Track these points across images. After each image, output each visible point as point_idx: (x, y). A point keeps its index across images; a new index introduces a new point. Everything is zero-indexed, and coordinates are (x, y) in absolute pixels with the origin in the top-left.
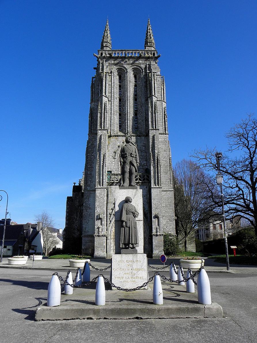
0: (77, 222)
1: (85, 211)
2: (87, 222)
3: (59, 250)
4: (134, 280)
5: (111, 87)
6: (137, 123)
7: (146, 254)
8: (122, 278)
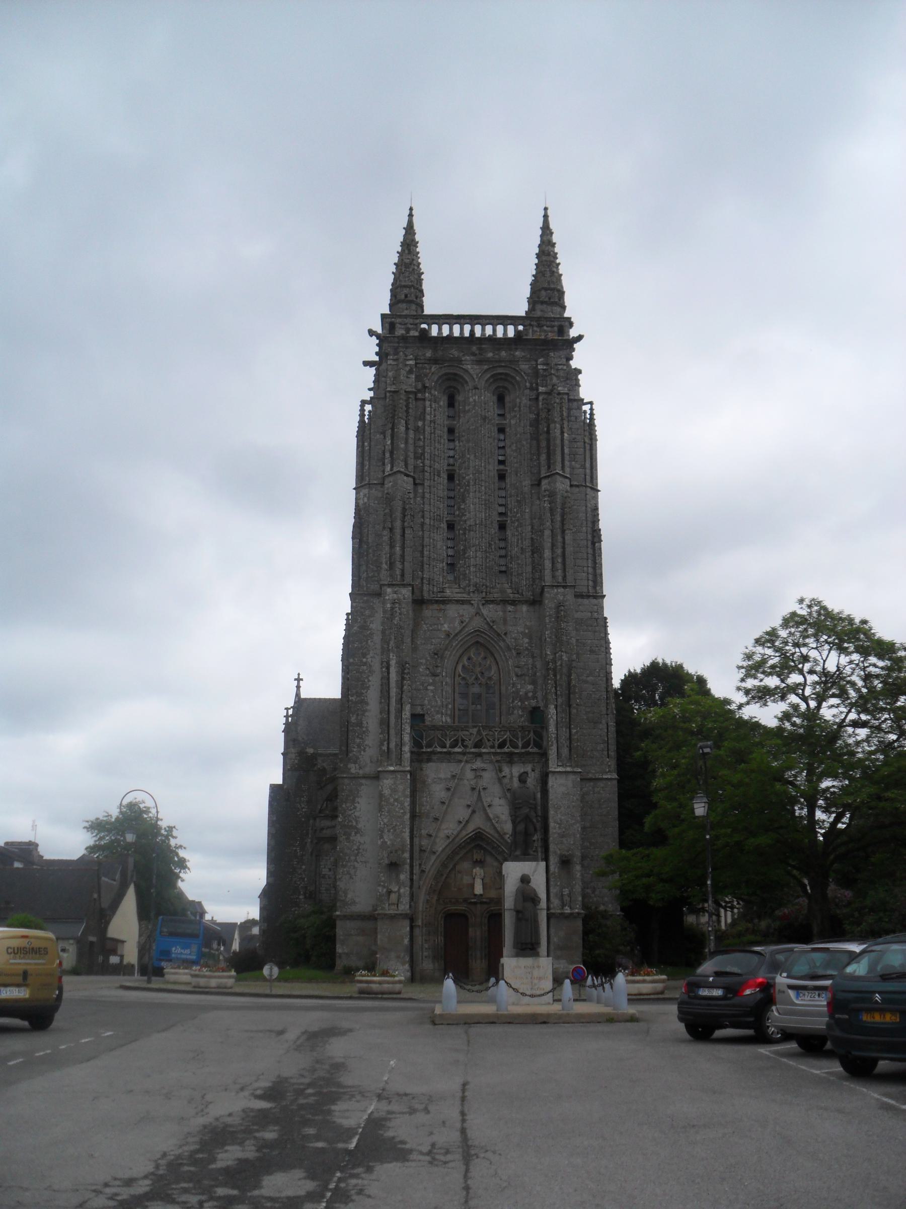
1: (342, 838)
2: (350, 874)
6: (505, 556)
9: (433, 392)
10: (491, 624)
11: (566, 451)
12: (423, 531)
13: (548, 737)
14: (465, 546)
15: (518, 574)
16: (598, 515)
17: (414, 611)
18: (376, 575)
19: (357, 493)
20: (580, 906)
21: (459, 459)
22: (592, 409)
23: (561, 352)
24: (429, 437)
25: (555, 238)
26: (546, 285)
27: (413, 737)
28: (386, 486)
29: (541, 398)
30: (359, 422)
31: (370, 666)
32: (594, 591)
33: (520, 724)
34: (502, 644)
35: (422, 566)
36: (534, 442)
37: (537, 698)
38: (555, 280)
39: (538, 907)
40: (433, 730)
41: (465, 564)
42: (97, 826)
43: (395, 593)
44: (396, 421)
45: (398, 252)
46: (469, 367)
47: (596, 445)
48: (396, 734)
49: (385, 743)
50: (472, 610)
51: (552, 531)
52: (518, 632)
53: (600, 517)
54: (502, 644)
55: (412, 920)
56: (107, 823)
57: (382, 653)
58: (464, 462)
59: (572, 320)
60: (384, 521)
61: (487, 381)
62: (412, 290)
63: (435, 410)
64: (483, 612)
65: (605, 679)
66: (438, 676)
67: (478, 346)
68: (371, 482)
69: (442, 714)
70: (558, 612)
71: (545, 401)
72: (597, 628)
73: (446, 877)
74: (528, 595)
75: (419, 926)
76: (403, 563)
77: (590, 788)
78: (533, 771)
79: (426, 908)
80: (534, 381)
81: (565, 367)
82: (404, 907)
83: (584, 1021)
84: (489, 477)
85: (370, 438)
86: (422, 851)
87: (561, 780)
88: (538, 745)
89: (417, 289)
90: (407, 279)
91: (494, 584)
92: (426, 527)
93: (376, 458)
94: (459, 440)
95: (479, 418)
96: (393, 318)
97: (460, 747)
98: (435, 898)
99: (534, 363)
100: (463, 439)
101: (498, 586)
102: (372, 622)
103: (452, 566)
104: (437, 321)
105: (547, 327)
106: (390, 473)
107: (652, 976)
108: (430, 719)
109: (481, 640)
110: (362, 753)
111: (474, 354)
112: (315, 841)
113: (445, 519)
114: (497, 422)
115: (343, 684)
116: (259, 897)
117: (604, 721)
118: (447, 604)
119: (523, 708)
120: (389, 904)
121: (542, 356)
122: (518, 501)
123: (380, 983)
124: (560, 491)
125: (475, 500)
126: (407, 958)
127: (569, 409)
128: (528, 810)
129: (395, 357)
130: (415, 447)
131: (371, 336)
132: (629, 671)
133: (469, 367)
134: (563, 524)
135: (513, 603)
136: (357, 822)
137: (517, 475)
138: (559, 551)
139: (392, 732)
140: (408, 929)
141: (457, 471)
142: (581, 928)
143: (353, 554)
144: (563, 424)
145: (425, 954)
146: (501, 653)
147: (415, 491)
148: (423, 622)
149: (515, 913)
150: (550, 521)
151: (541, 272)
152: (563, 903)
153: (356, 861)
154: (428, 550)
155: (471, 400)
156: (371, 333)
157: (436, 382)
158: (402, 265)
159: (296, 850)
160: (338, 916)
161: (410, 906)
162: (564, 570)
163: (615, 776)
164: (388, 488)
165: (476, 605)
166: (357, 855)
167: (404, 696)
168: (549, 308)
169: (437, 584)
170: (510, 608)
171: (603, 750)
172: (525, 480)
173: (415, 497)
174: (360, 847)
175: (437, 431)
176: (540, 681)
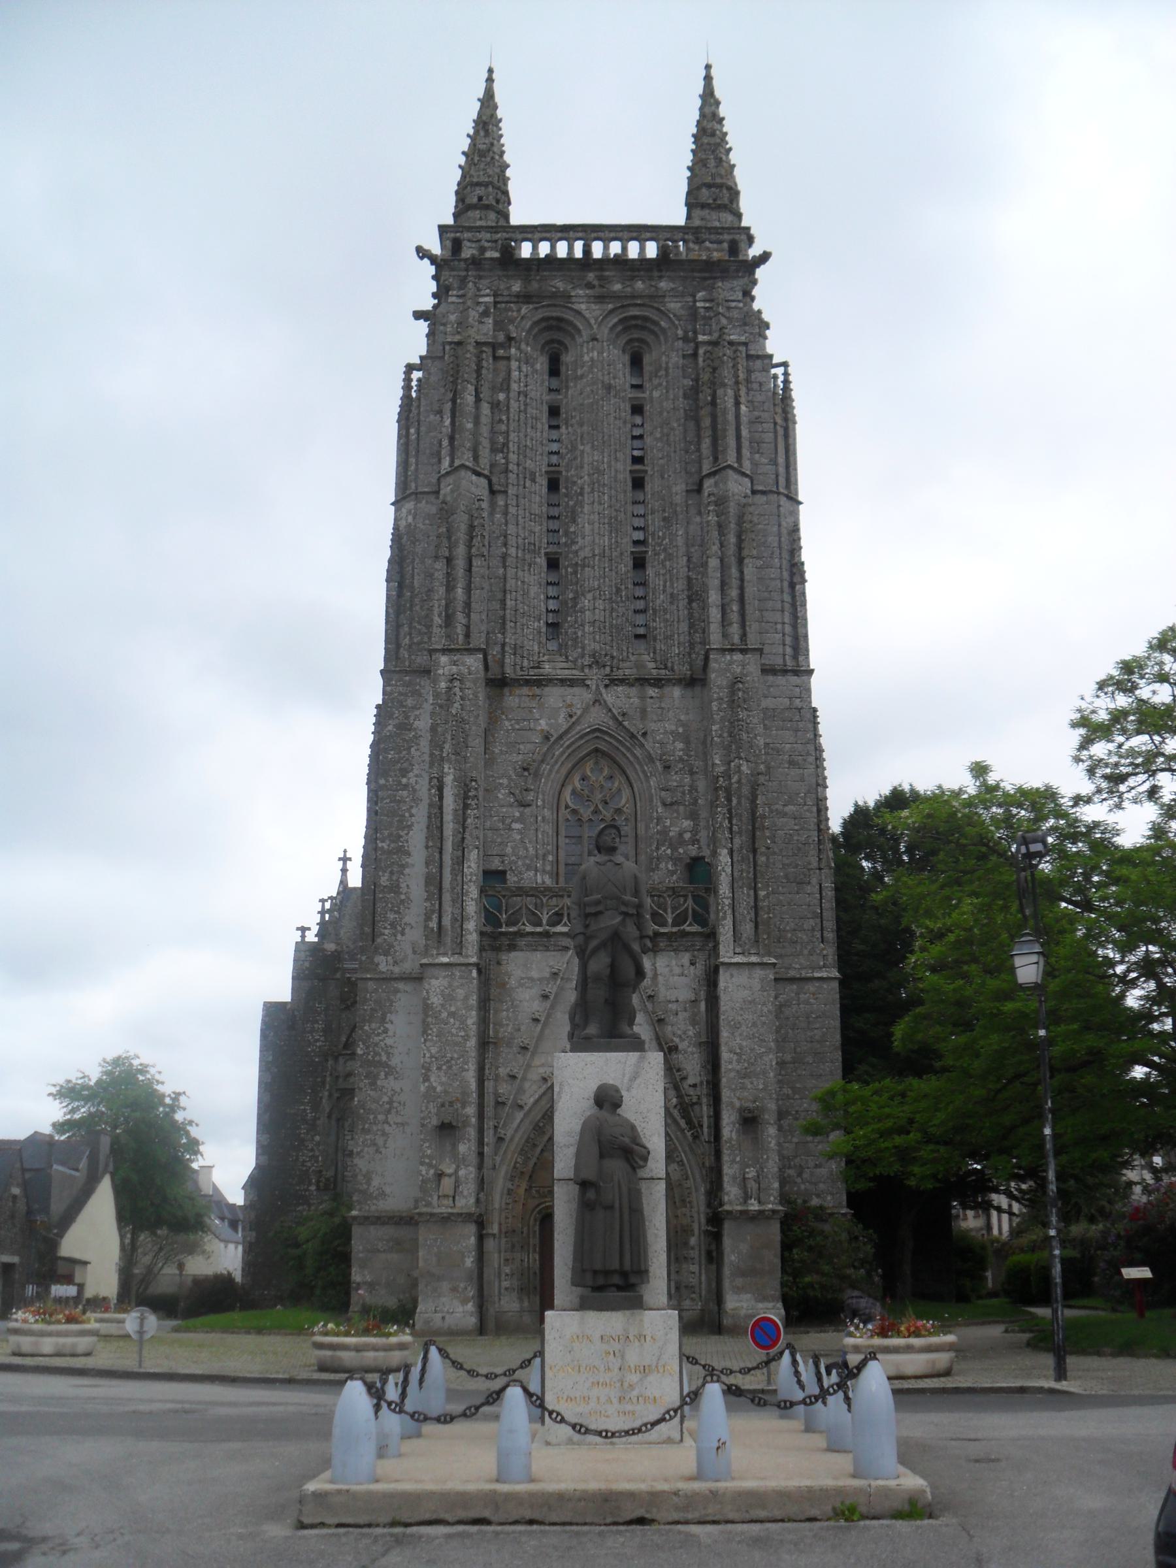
0: (317, 1138)
2: (375, 1144)
3: (224, 1281)
4: (629, 1407)
5: (508, 420)
7: (289, 1000)
8: (586, 1399)
9: (523, 346)
10: (620, 719)
11: (745, 433)
12: (505, 567)
13: (718, 904)
14: (576, 592)
15: (666, 638)
16: (799, 539)
17: (489, 697)
18: (426, 639)
19: (396, 511)
20: (775, 1198)
21: (567, 453)
22: (786, 374)
23: (735, 282)
24: (517, 418)
25: (723, 111)
26: (709, 180)
27: (485, 907)
28: (442, 492)
29: (701, 351)
30: (401, 399)
31: (415, 791)
32: (794, 664)
33: (672, 885)
34: (638, 752)
35: (504, 623)
36: (691, 425)
37: (698, 841)
38: (723, 172)
39: (642, 1173)
40: (520, 896)
41: (576, 622)
42: (69, 1092)
43: (455, 663)
44: (459, 387)
45: (468, 135)
46: (583, 307)
47: (794, 429)
48: (453, 901)
49: (435, 917)
50: (588, 696)
51: (722, 561)
52: (666, 732)
53: (803, 543)
54: (638, 752)
55: (481, 1223)
56: (85, 1087)
57: (431, 765)
58: (575, 458)
59: (752, 232)
60: (438, 547)
61: (612, 329)
62: (490, 189)
63: (526, 376)
64: (607, 699)
65: (815, 809)
66: (529, 805)
67: (597, 273)
68: (420, 490)
69: (536, 870)
70: (733, 692)
71: (708, 355)
72: (801, 725)
73: (542, 1150)
74: (683, 670)
75: (494, 1235)
76: (468, 616)
77: (793, 995)
78: (692, 964)
79: (507, 1204)
80: (690, 327)
81: (741, 305)
82: (466, 1202)
83: (763, 1514)
84: (616, 481)
85: (419, 421)
86: (499, 1104)
87: (741, 978)
88: (701, 919)
89: (499, 188)
90: (481, 173)
91: (625, 654)
92: (509, 561)
93: (428, 451)
94: (566, 424)
95: (600, 386)
96: (457, 232)
97: (565, 925)
98: (524, 1185)
99: (690, 299)
100: (574, 421)
101: (632, 658)
102: (417, 718)
103: (554, 627)
104: (529, 236)
105: (711, 243)
106: (449, 469)
107: (924, 1336)
108: (516, 879)
109: (602, 746)
110: (399, 937)
111: (590, 286)
112: (336, 1095)
113: (543, 551)
114: (630, 396)
115: (368, 820)
116: (243, 1188)
117: (814, 881)
118: (545, 686)
119: (676, 860)
120: (439, 1197)
121: (704, 289)
122: (664, 519)
123: (358, 1349)
124: (733, 495)
125: (592, 517)
126: (471, 1292)
127: (749, 371)
128: (619, 919)
129: (461, 292)
130: (493, 432)
131: (422, 258)
132: (856, 805)
133: (583, 307)
134: (740, 548)
135: (658, 683)
136: (388, 1054)
137: (663, 478)
138: (734, 593)
139: (447, 897)
140: (473, 1240)
141: (564, 473)
142: (778, 1237)
143: (387, 607)
144: (739, 390)
145: (505, 1284)
146: (637, 767)
147: (493, 505)
148: (504, 717)
149: (577, 1187)
150: (717, 542)
151: (701, 160)
152: (746, 1193)
153: (386, 1122)
154: (513, 598)
155: (586, 358)
156: (422, 253)
157: (529, 332)
158: (474, 154)
159: (305, 1110)
160: (355, 1218)
161: (478, 1201)
162: (743, 625)
163: (835, 973)
164: (445, 495)
165: (594, 687)
166: (389, 1111)
167: (467, 835)
168: (714, 215)
169: (529, 654)
170: (652, 692)
171: (813, 930)
172: (676, 485)
173: (492, 514)
174: (394, 1099)
175: (529, 410)
176: (704, 814)
